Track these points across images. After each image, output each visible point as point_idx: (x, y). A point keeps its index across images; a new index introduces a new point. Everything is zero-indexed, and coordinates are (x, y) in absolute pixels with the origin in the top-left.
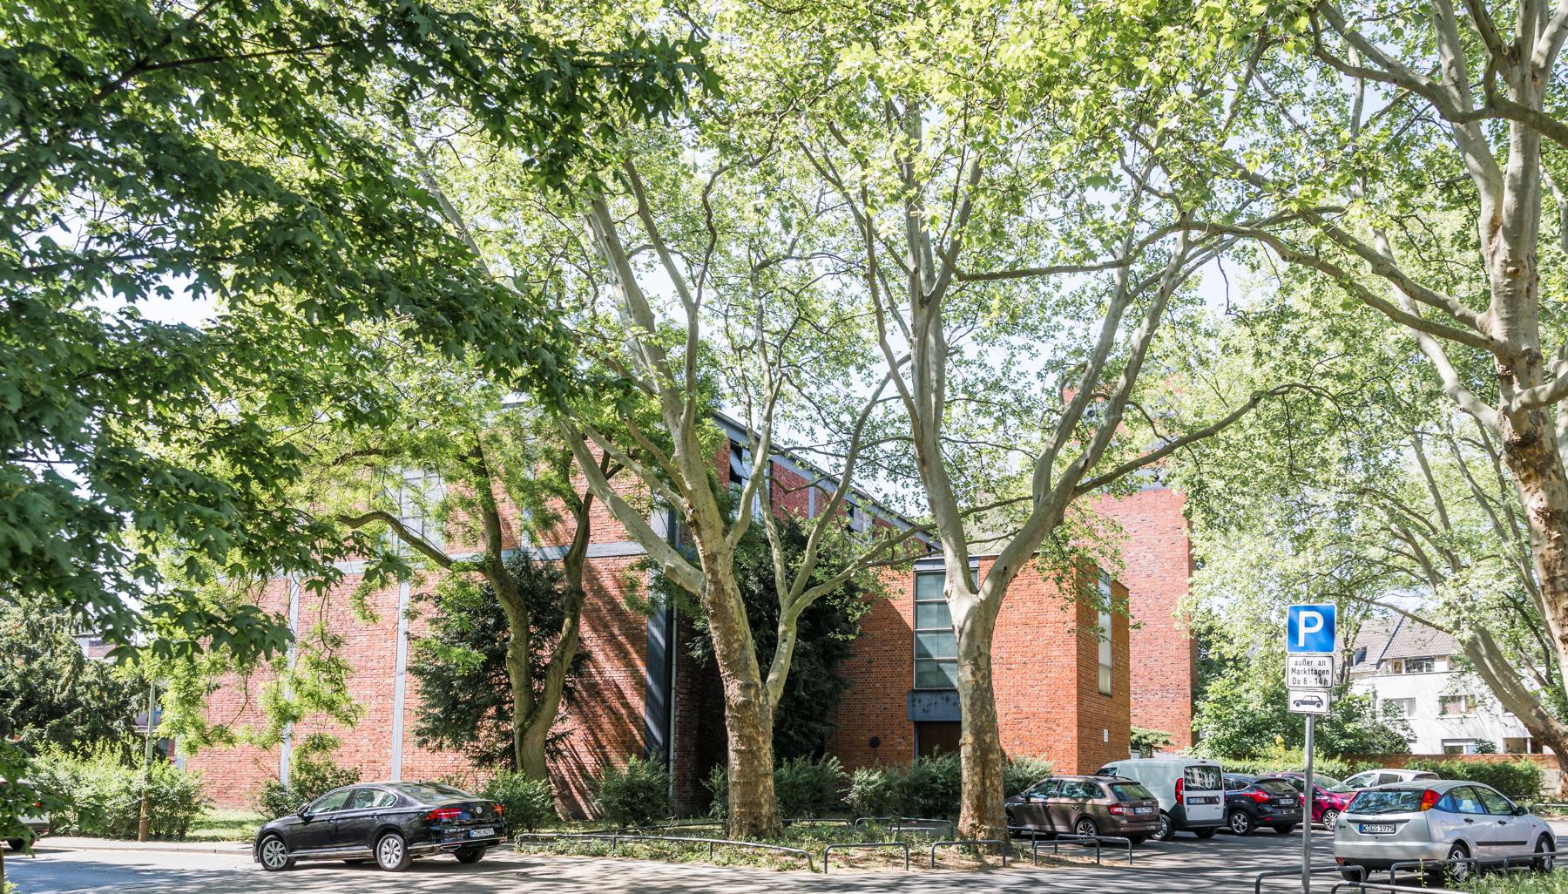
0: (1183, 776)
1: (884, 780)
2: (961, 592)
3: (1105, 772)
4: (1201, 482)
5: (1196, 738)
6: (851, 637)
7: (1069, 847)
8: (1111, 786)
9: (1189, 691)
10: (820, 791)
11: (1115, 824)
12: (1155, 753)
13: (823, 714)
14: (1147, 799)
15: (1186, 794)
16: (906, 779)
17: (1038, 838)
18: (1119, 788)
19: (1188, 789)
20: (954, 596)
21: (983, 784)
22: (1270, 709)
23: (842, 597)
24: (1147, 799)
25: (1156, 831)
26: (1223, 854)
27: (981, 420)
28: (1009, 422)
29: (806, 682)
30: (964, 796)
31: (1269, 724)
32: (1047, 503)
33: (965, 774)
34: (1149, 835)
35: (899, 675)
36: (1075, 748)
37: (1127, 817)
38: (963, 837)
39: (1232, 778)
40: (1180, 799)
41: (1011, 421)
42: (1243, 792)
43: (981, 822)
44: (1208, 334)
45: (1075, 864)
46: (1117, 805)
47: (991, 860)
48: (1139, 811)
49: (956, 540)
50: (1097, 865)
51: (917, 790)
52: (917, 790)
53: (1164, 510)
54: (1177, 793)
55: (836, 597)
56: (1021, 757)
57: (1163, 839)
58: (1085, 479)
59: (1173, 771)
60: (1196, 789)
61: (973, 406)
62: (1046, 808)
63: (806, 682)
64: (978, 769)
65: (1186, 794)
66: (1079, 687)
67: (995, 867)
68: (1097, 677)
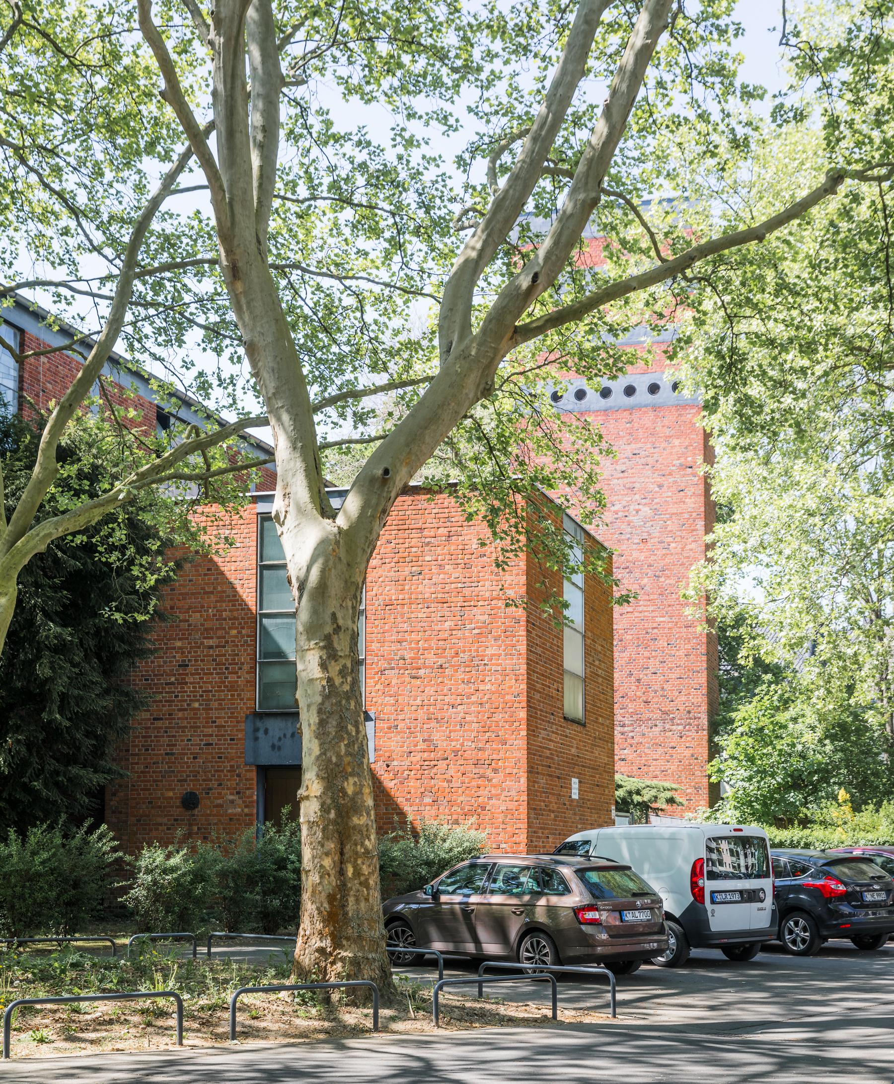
0: (703, 854)
1: (191, 865)
2: (300, 511)
3: (572, 848)
4: (733, 350)
5: (715, 794)
6: (140, 618)
7: (506, 985)
8: (581, 873)
9: (704, 722)
10: (76, 885)
11: (587, 941)
12: (653, 818)
13: (98, 752)
14: (642, 894)
15: (709, 885)
16: (232, 864)
17: (450, 964)
18: (594, 877)
19: (713, 876)
20: (290, 522)
21: (342, 873)
22: (829, 748)
23: (123, 549)
24: (642, 894)
25: (659, 952)
26: (777, 993)
27: (362, 243)
28: (409, 248)
29: (63, 697)
30: (306, 896)
31: (826, 773)
32: (464, 355)
33: (307, 853)
34: (647, 957)
35: (233, 687)
36: (524, 809)
37: (608, 929)
38: (303, 973)
39: (784, 857)
40: (698, 893)
41: (415, 245)
42: (804, 880)
43: (337, 945)
44: (748, 94)
45: (512, 1021)
46: (591, 908)
47: (351, 1017)
48: (629, 916)
49: (295, 418)
50: (550, 1022)
51: (251, 881)
52: (251, 881)
53: (667, 438)
54: (694, 885)
55: (112, 548)
56: (432, 824)
57: (670, 964)
58: (537, 311)
59: (685, 845)
60: (726, 876)
61: (348, 214)
62: (467, 913)
63: (63, 697)
64: (331, 845)
65: (709, 885)
66: (530, 707)
67: (357, 1032)
68: (559, 691)
